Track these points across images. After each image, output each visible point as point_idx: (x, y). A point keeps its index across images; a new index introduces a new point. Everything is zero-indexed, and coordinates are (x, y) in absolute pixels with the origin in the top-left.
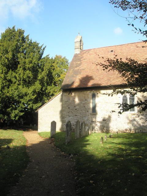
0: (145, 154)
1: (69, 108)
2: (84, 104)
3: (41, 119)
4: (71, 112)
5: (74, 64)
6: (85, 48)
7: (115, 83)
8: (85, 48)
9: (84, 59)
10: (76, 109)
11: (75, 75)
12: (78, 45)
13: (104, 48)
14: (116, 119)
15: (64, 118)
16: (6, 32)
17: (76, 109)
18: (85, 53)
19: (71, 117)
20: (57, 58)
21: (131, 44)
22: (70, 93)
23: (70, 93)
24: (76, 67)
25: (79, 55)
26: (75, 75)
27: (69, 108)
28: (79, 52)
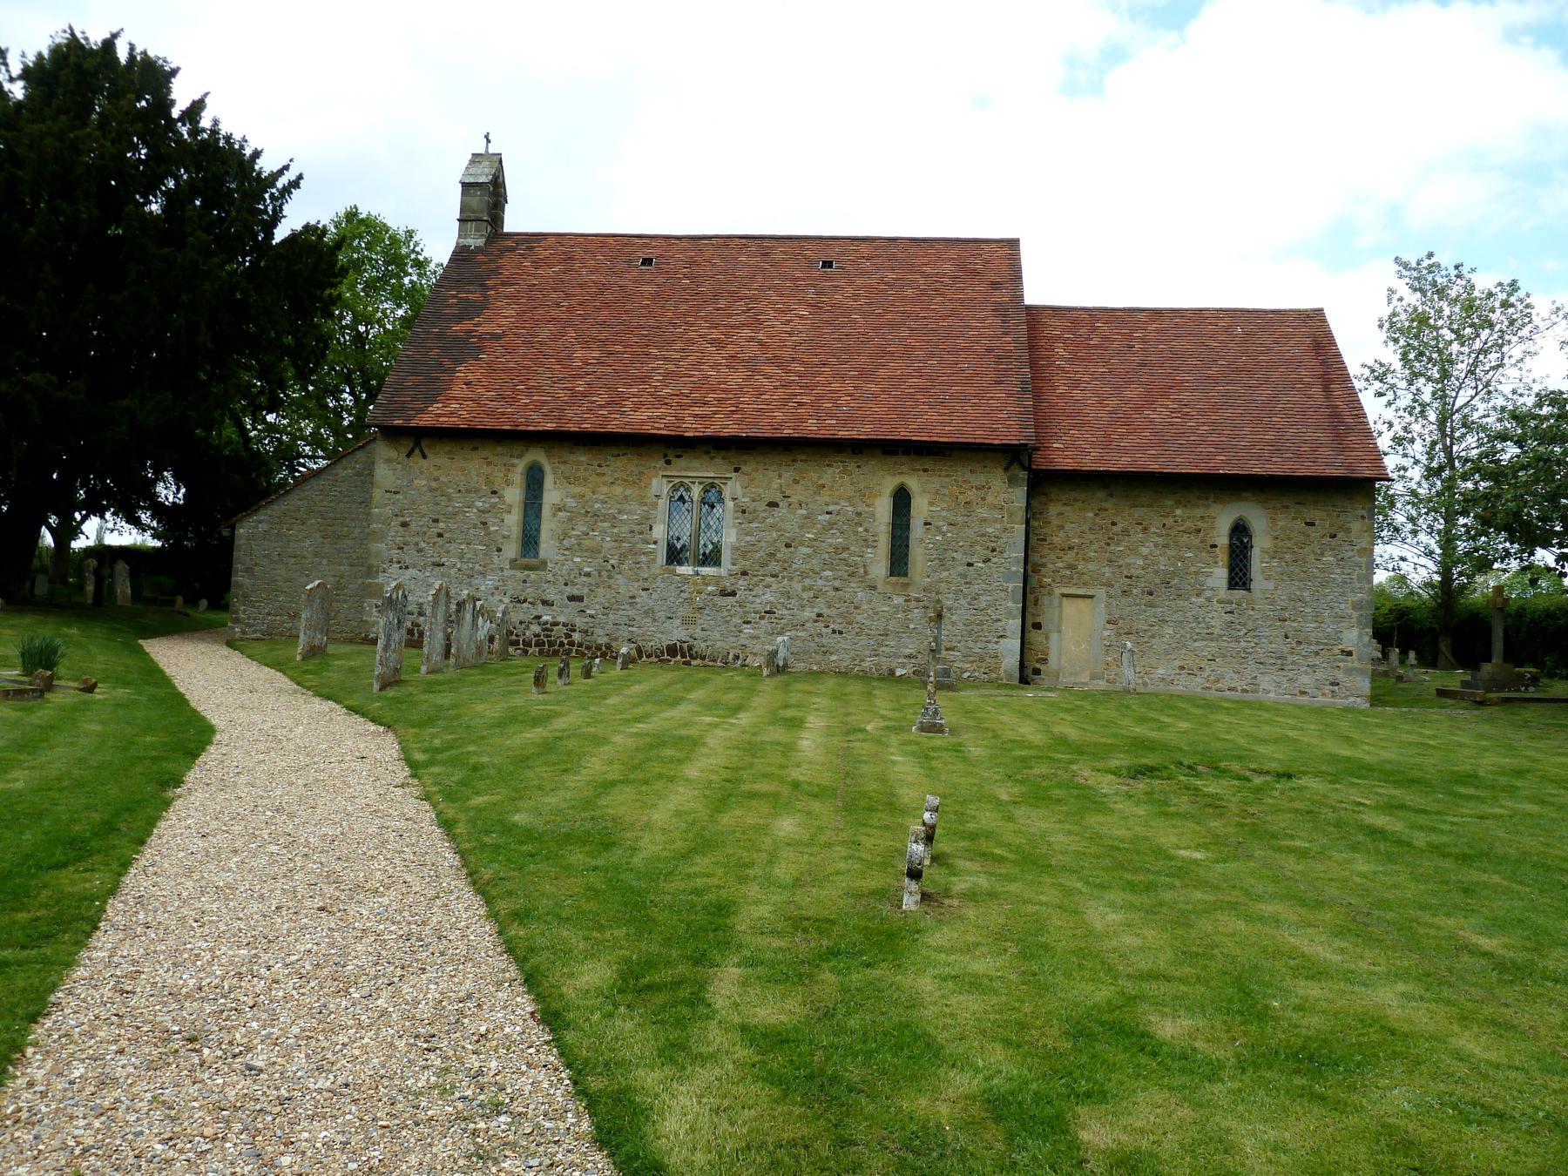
0: (784, 898)
1: (404, 525)
2: (483, 512)
3: (615, 403)
4: (417, 544)
5: (446, 299)
6: (514, 222)
7: (643, 422)
8: (514, 222)
9: (504, 284)
10: (440, 535)
11: (447, 363)
12: (856, 688)
13: (611, 240)
14: (634, 597)
15: (377, 572)
16: (56, 51)
17: (440, 535)
18: (512, 250)
19: (412, 572)
20: (307, 228)
21: (744, 241)
22: (417, 451)
23: (417, 451)
24: (460, 318)
25: (480, 258)
26: (447, 363)
27: (404, 525)
28: (480, 242)
